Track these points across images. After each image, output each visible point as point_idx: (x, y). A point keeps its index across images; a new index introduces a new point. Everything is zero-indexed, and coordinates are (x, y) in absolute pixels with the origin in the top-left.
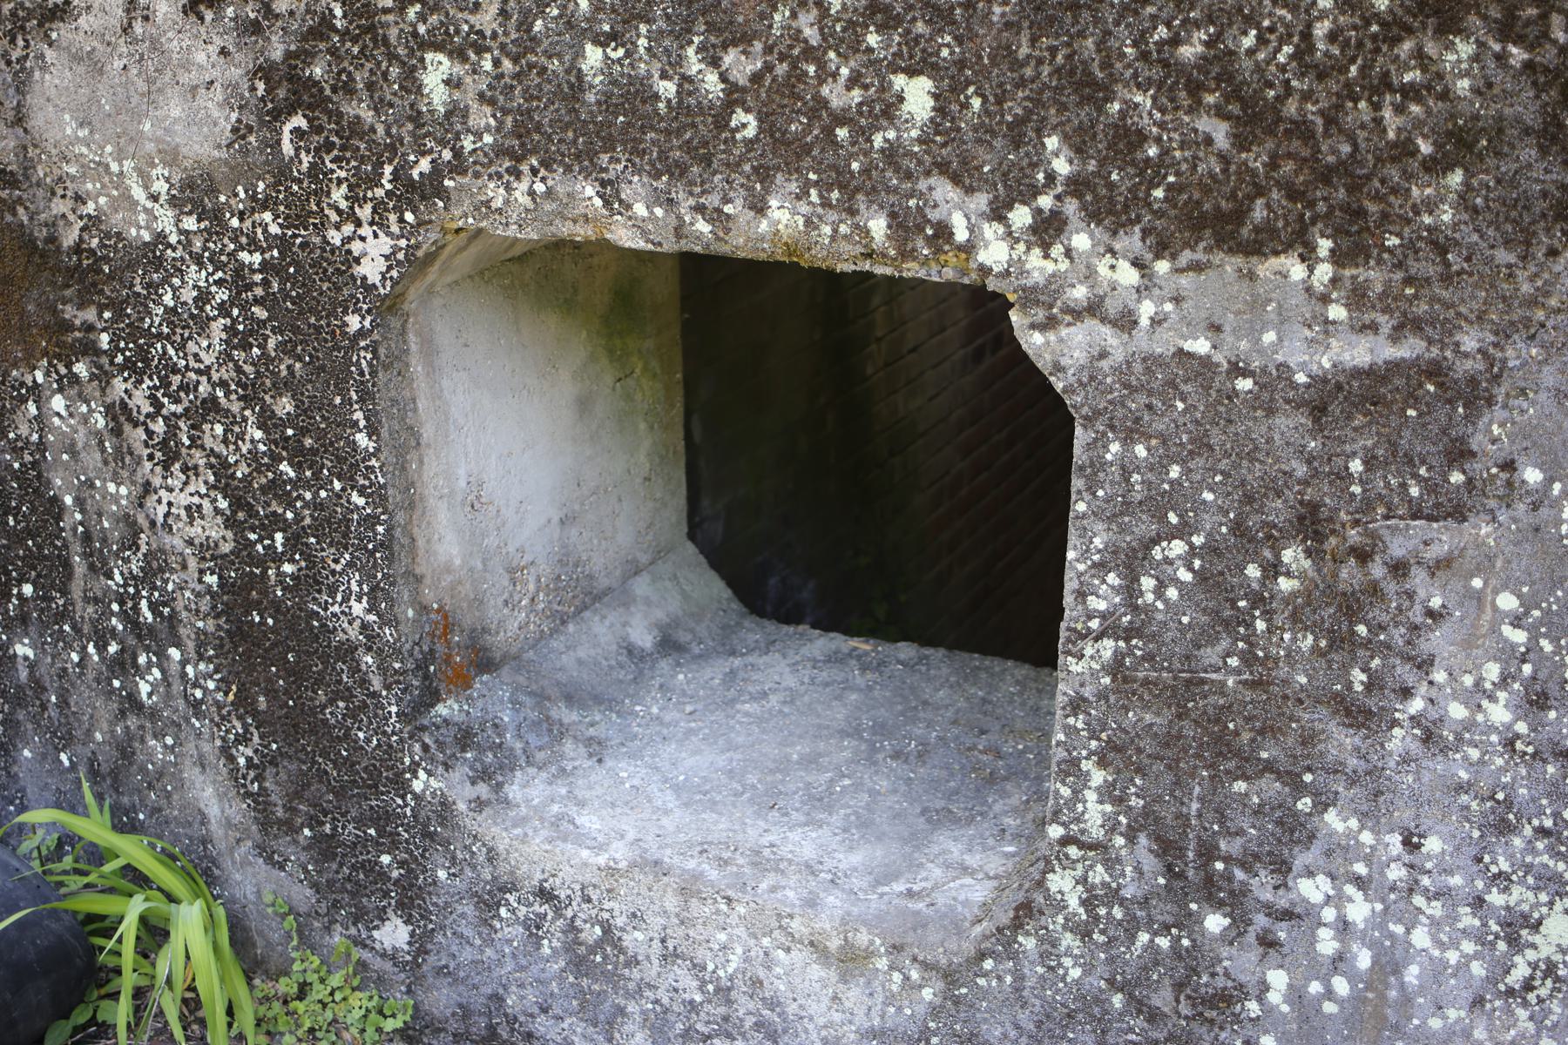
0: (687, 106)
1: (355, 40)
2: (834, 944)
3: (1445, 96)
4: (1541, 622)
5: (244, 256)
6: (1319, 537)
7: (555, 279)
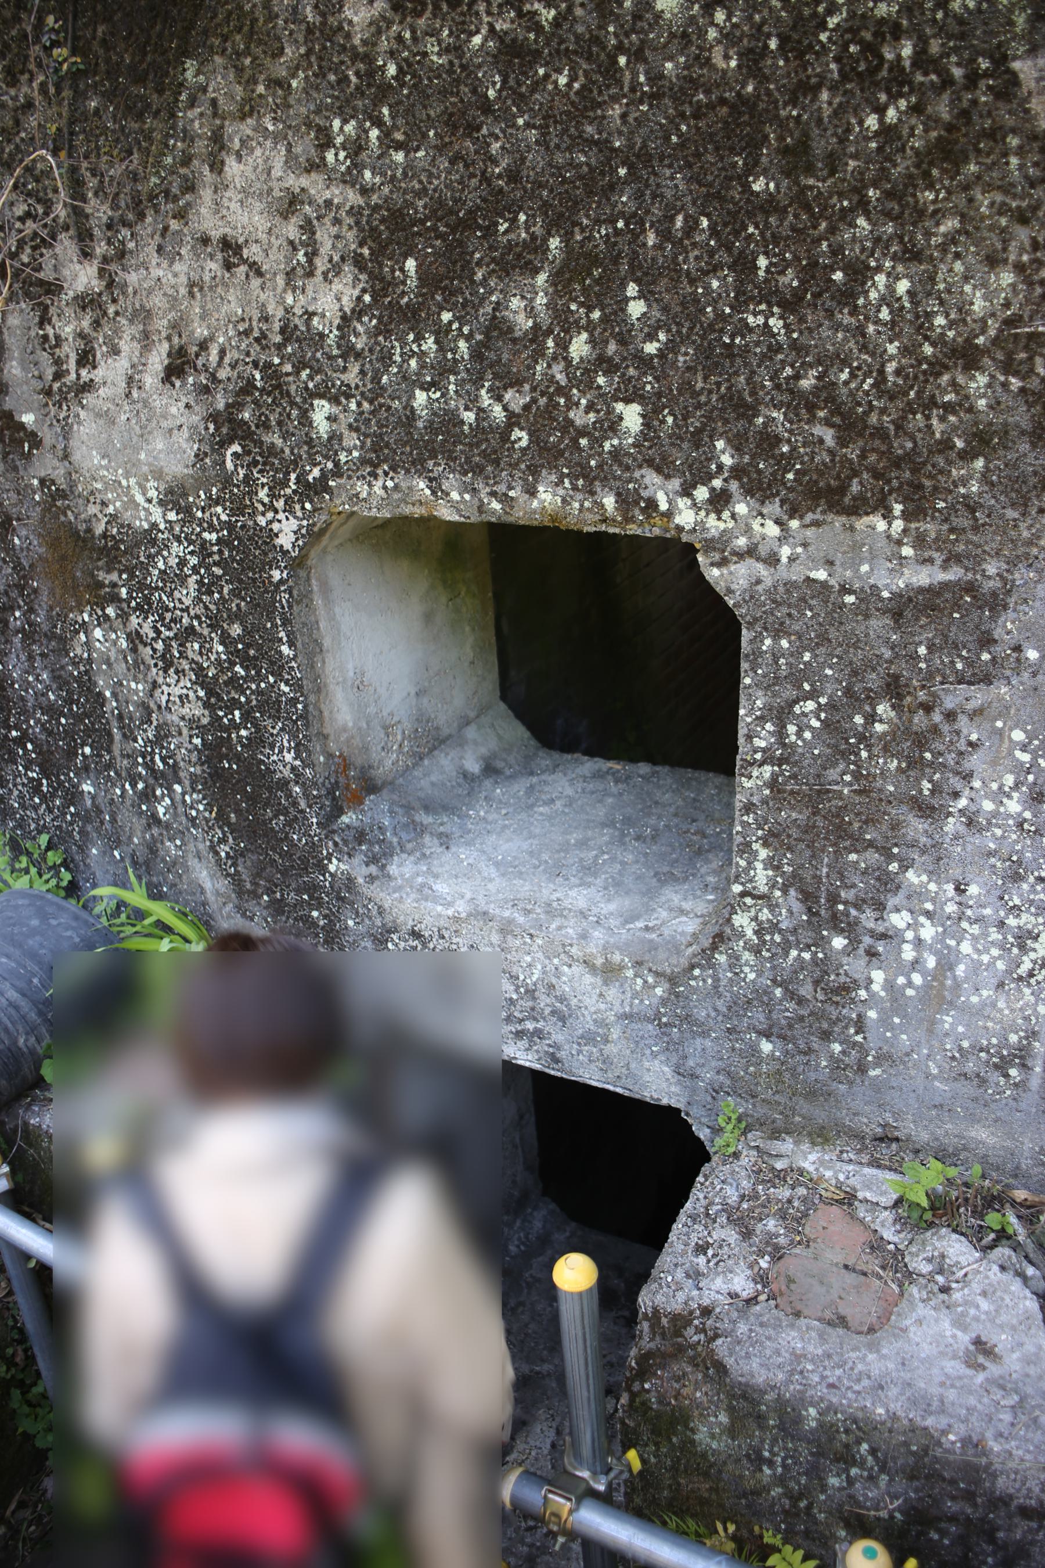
0: (483, 427)
1: (269, 394)
2: (599, 961)
3: (971, 410)
4: (1039, 748)
5: (206, 535)
6: (900, 697)
7: (402, 539)
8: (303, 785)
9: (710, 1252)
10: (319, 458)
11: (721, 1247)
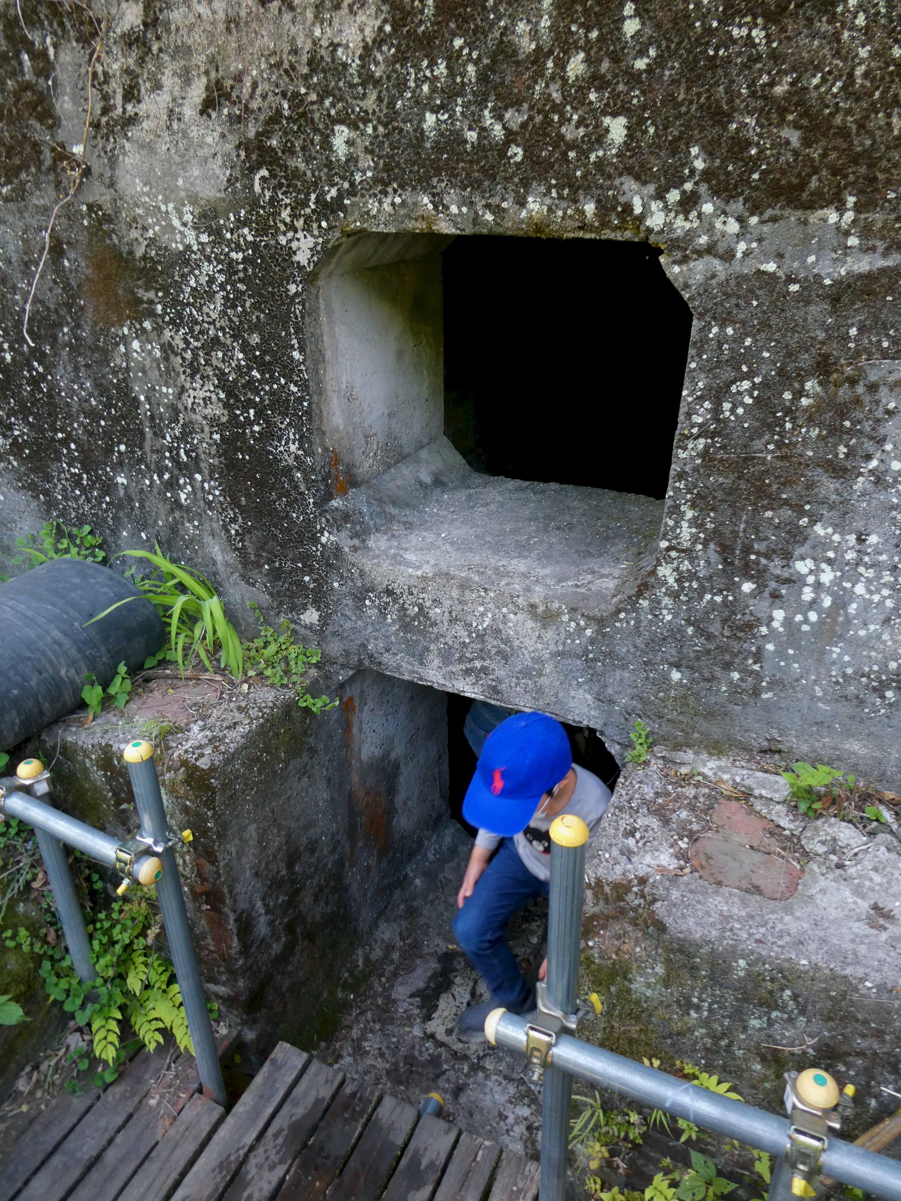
1: (295, 123)
2: (541, 609)
5: (233, 255)
6: (828, 373)
8: (304, 472)
9: (638, 835)
10: (336, 179)
11: (646, 831)
